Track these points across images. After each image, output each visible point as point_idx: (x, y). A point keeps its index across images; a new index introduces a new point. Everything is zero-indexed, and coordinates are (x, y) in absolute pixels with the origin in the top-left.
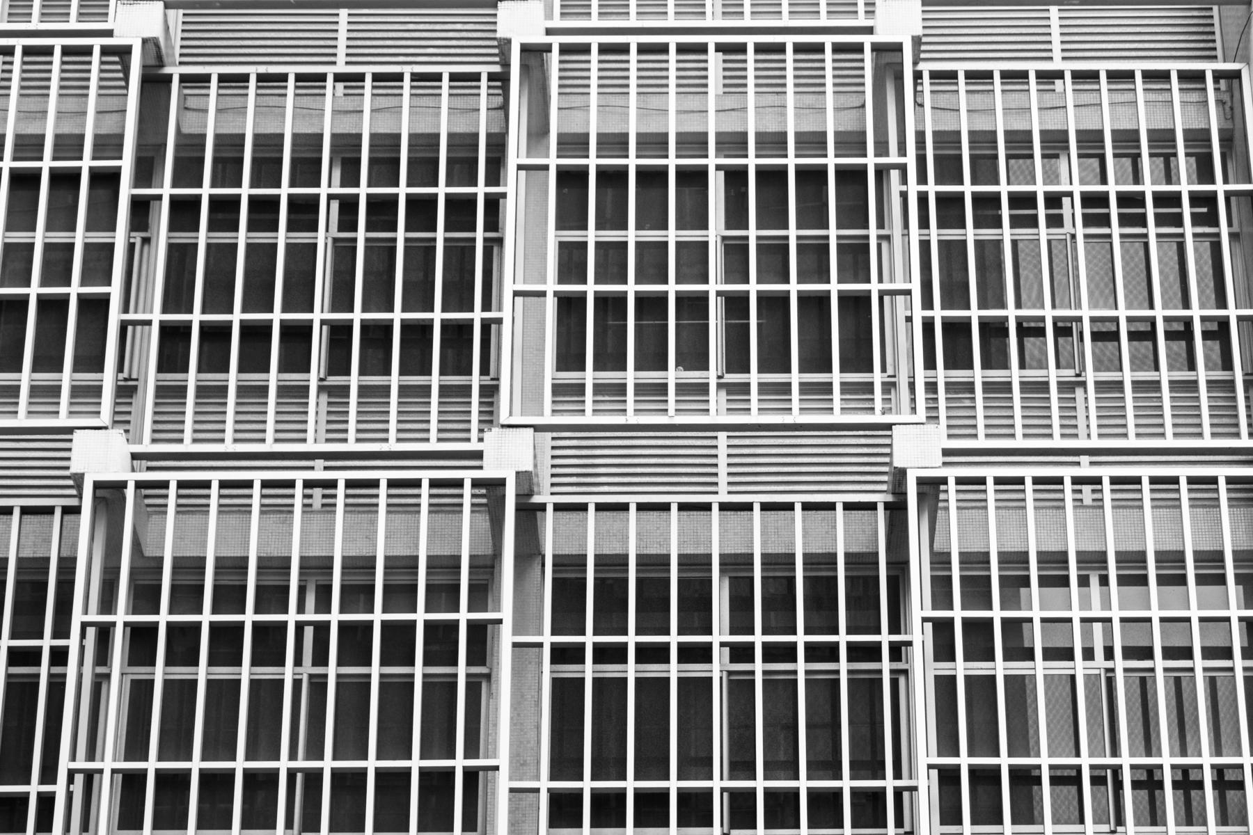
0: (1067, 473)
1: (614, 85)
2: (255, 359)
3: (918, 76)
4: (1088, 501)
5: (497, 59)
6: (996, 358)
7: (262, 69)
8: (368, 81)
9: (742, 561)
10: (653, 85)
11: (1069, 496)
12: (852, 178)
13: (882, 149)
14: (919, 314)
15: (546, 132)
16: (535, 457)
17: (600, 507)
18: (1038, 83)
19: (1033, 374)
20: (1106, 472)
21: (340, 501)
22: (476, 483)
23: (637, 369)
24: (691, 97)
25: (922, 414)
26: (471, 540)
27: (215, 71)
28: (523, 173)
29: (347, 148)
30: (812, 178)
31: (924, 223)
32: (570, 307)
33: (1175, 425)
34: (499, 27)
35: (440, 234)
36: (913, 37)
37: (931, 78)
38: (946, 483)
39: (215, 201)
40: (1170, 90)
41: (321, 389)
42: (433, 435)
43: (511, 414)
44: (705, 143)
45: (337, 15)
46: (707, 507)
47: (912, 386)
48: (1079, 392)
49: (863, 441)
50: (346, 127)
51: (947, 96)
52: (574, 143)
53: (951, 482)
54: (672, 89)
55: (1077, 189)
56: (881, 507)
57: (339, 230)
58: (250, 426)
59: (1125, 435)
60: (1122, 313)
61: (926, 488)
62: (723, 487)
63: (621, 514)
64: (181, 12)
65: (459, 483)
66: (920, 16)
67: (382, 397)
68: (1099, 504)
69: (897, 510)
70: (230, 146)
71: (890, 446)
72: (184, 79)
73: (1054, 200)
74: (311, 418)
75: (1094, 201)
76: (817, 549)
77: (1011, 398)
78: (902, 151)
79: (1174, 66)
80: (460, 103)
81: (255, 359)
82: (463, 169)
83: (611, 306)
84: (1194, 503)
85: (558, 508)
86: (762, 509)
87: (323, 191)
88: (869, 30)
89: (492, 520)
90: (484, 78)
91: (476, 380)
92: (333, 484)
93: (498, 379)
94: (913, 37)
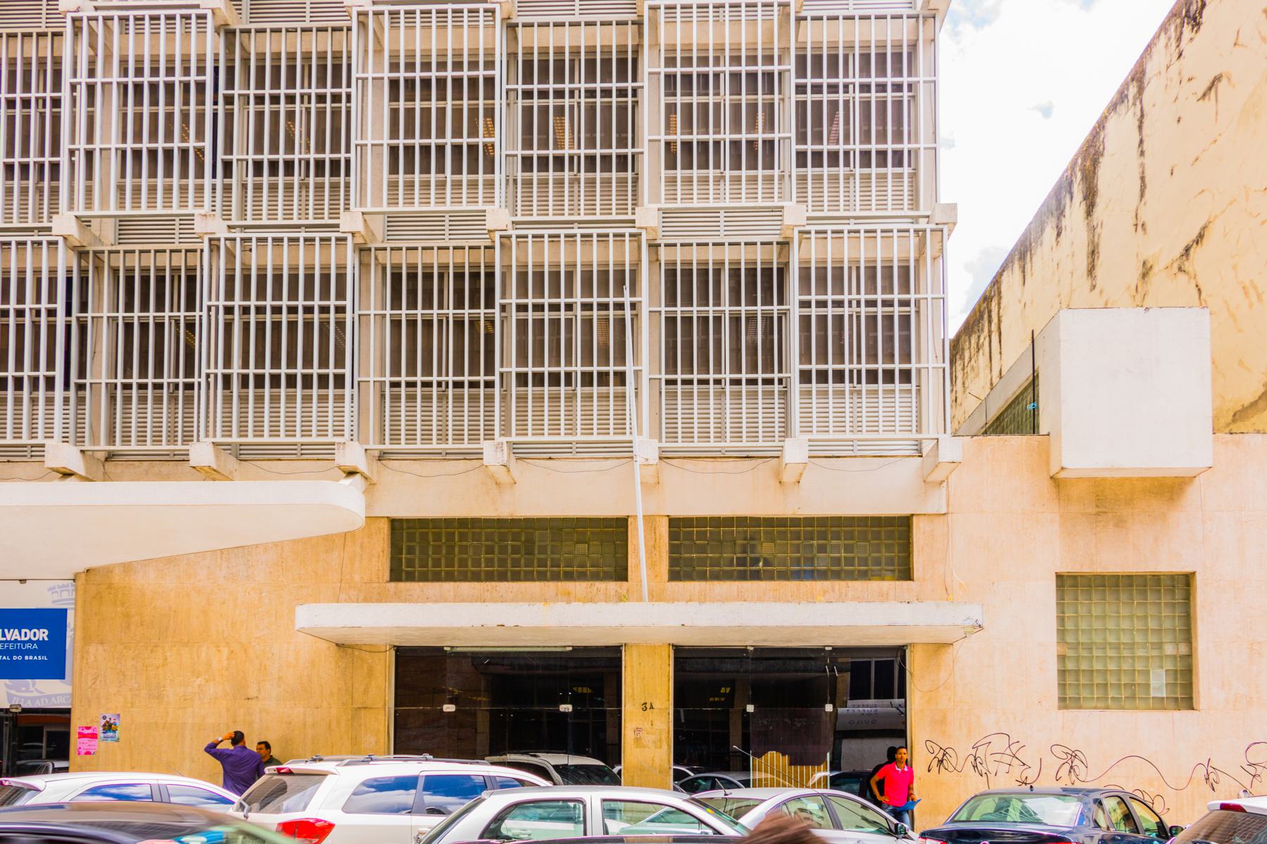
32: (394, 150)
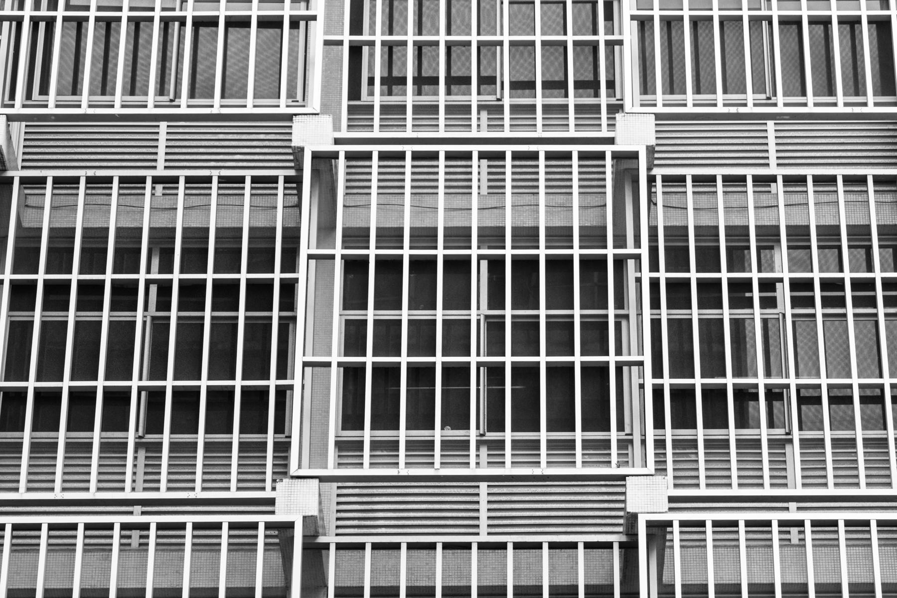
0: (775, 517)
1: (391, 187)
2: (81, 419)
3: (651, 180)
4: (795, 541)
5: (292, 164)
6: (716, 419)
7: (91, 173)
8: (248, 184)
9: (497, 592)
10: (425, 187)
11: (776, 536)
12: (594, 267)
13: (620, 241)
14: (650, 382)
15: (333, 228)
16: (320, 503)
17: (376, 547)
18: (754, 186)
19: (748, 433)
20: (808, 517)
21: (152, 541)
22: (269, 526)
23: (408, 428)
24: (459, 197)
25: (651, 467)
26: (263, 574)
27: (50, 174)
28: (313, 262)
29: (162, 240)
30: (560, 267)
31: (655, 304)
32: (353, 375)
33: (867, 476)
34: (293, 137)
35: (242, 313)
36: (647, 147)
37: (663, 181)
38: (671, 526)
39: (218, 285)
40: (867, 192)
41: (138, 446)
42: (198, 484)
43: (300, 467)
44: (401, 236)
45: (158, 126)
46: (467, 546)
47: (644, 442)
48: (788, 447)
49: (604, 490)
50: (162, 222)
51: (736, 196)
52: (356, 236)
53: (676, 525)
54: (441, 190)
55: (787, 276)
56: (616, 547)
57: (157, 310)
58: (76, 477)
59: (762, 485)
60: (824, 381)
61: (654, 530)
62: (484, 529)
63: (395, 552)
64: (24, 124)
65: (254, 526)
66: (653, 128)
67: (190, 452)
68: (802, 544)
69: (629, 548)
70: (62, 239)
71: (624, 494)
72: (24, 181)
73: (768, 285)
74: (129, 469)
75: (801, 286)
76: (561, 581)
77: (761, 453)
78: (638, 244)
79: (870, 172)
80: (259, 201)
81: (81, 419)
82: (262, 258)
83: (387, 375)
84: (883, 543)
85: (340, 547)
86: (585, 548)
87: (142, 277)
88: (611, 141)
89: (283, 557)
90: (281, 180)
91: (270, 437)
92: (146, 527)
93: (290, 437)
94: (647, 147)
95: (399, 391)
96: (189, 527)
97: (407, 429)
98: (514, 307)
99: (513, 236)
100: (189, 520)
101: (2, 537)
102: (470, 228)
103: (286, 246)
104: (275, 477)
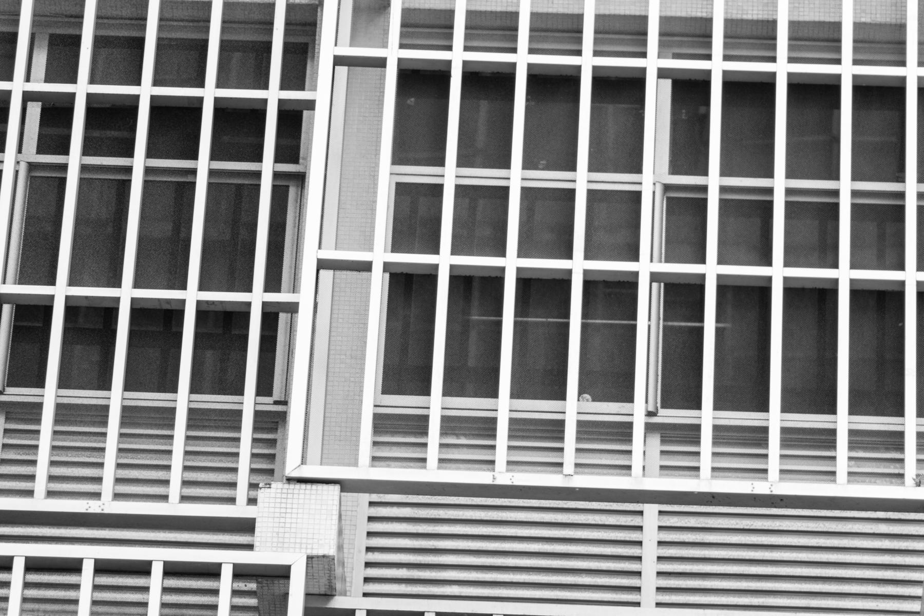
16: (340, 532)
22: (241, 572)
28: (342, 71)
43: (303, 462)
57: (40, 151)
65: (212, 572)
67: (93, 424)
93: (285, 403)
95: (499, 324)
96: (88, 568)
97: (513, 396)
98: (791, 173)
99: (792, 39)
100: (89, 554)
101: (6, 584)
102: (774, 23)
103: (292, 40)
104: (256, 479)
